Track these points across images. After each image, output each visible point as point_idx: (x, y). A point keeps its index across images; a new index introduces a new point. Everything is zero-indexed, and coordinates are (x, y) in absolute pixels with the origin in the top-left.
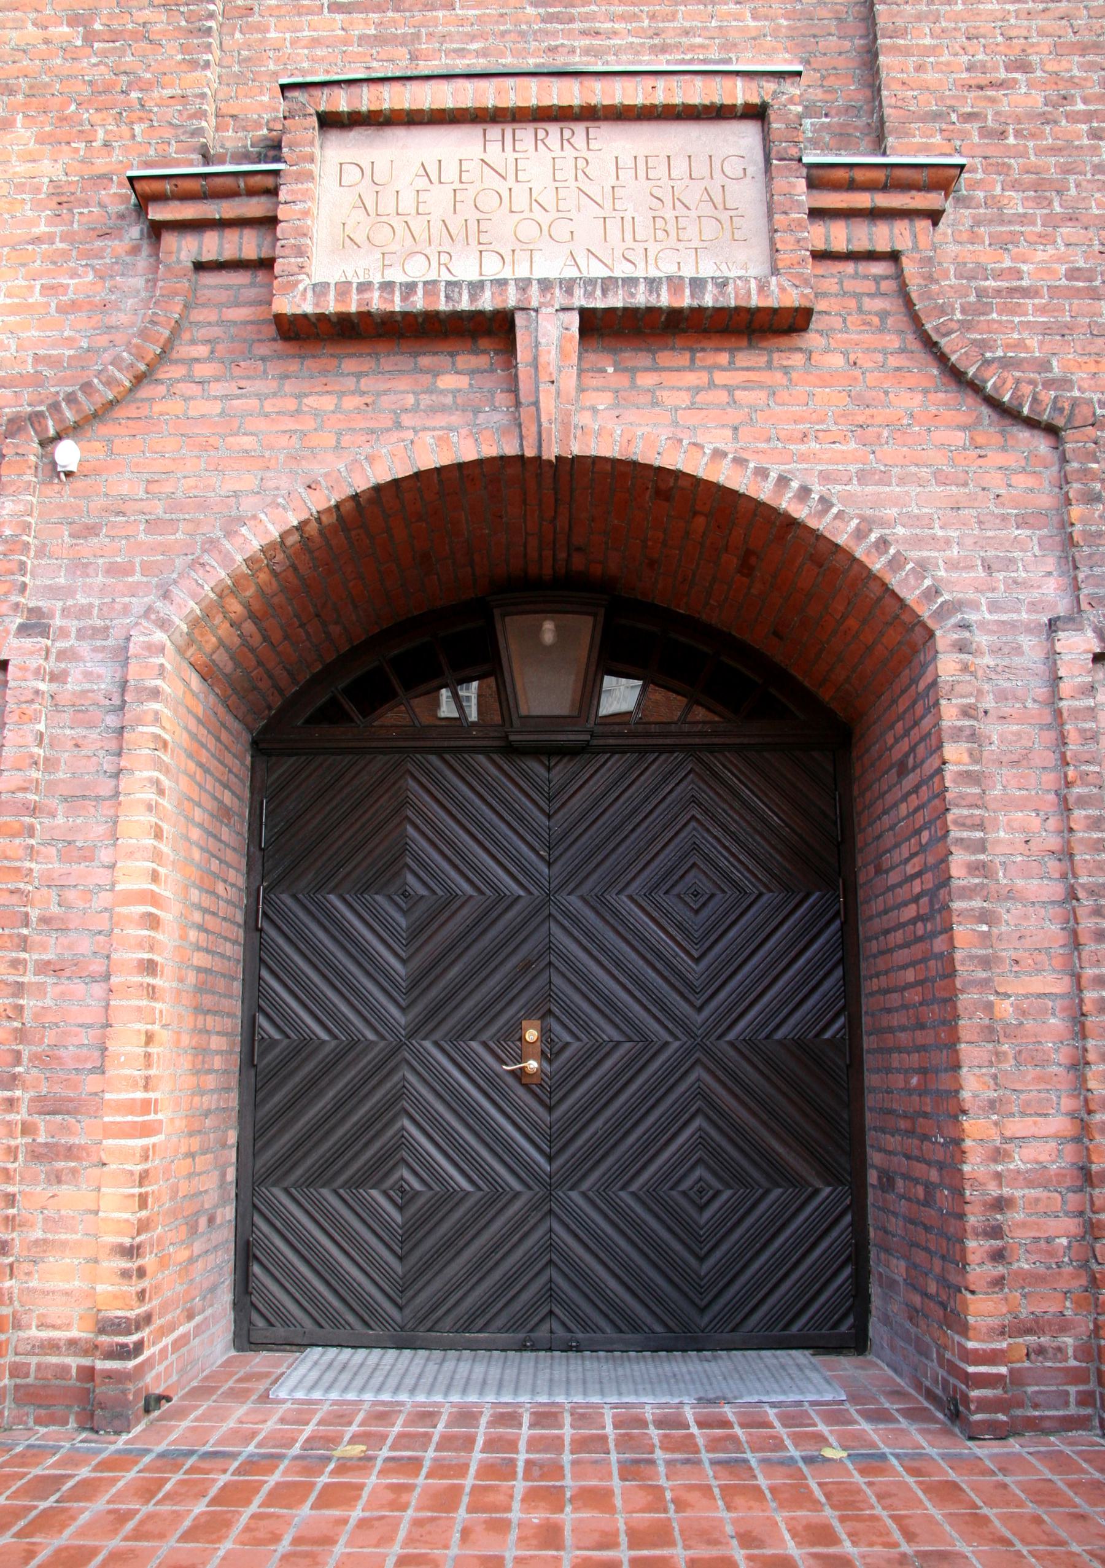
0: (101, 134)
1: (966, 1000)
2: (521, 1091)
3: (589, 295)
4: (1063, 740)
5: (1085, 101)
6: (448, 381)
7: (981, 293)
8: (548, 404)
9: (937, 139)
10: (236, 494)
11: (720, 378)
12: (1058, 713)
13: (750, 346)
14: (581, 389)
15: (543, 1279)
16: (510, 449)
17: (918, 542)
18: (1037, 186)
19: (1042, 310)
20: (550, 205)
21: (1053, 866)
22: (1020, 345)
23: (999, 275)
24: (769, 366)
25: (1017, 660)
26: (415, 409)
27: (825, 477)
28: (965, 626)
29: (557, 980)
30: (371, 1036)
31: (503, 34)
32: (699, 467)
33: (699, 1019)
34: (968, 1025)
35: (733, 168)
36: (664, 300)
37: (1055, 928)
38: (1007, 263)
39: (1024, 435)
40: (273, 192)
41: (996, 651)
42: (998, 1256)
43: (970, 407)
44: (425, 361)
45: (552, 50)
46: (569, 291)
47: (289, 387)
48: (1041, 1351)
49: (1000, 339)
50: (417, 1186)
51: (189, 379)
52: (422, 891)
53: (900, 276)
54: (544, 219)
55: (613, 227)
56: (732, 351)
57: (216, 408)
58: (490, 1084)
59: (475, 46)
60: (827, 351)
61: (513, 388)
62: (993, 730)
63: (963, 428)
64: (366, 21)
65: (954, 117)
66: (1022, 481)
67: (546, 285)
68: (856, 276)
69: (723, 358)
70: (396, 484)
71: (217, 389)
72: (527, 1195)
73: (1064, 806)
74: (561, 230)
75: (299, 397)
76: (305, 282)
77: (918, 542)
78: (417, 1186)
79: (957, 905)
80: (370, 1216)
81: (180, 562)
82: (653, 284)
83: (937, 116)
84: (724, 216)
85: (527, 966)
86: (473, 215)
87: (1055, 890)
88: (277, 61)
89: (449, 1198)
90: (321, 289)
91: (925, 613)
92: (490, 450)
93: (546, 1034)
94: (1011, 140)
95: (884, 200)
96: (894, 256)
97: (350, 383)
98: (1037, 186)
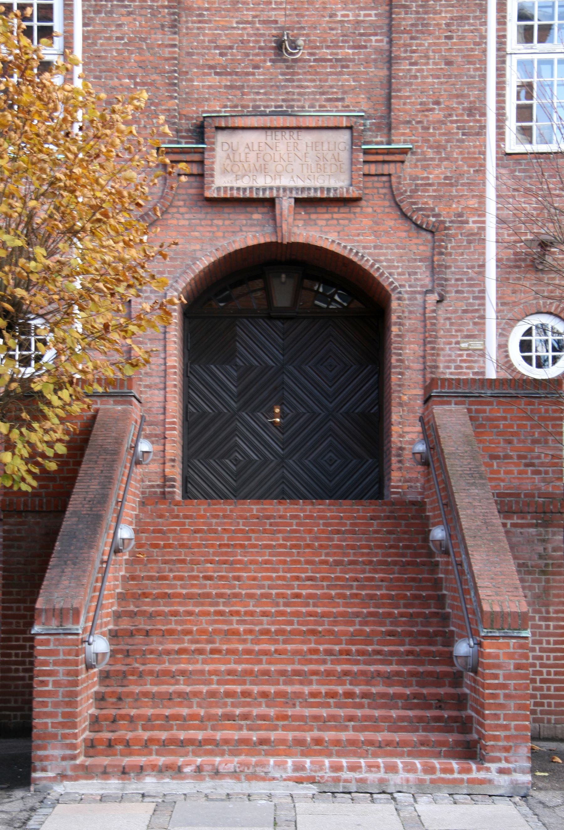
0: (143, 122)
1: (394, 395)
2: (274, 428)
3: (297, 193)
4: (425, 326)
5: (457, 116)
6: (256, 216)
7: (417, 185)
8: (285, 227)
9: (408, 131)
10: (195, 251)
11: (335, 216)
12: (425, 317)
13: (345, 206)
14: (295, 220)
15: (281, 487)
16: (274, 240)
17: (389, 267)
18: (438, 147)
19: (434, 191)
20: (286, 159)
21: (421, 360)
22: (426, 203)
23: (423, 179)
24: (350, 212)
25: (416, 302)
26: (246, 225)
27: (364, 248)
28: (400, 293)
29: (286, 393)
30: (225, 411)
31: (272, 86)
32: (327, 245)
33: (331, 405)
34: (394, 402)
35: (342, 146)
36: (319, 195)
37: (420, 377)
38: (425, 175)
39: (424, 233)
40: (203, 153)
41: (410, 299)
42: (400, 462)
43: (407, 225)
44: (249, 209)
45: (287, 93)
46: (291, 192)
47: (208, 217)
48: (411, 487)
49: (420, 201)
50: (241, 458)
51: (178, 212)
52: (242, 364)
53: (390, 181)
54: (284, 164)
55: (305, 167)
56: (339, 207)
57: (186, 223)
58: (264, 426)
59: (262, 91)
60: (367, 207)
61: (274, 218)
62: (407, 322)
63: (405, 231)
64: (226, 79)
65: (414, 122)
66: (422, 248)
67: (285, 189)
68: (378, 181)
69: (336, 209)
70: (241, 249)
71: (187, 216)
72: (275, 461)
73: (425, 344)
74: (289, 168)
75: (212, 220)
76: (214, 186)
77: (389, 267)
78: (241, 458)
79: (393, 370)
80: (226, 468)
81: (179, 271)
82: (316, 189)
83: (409, 122)
84: (338, 163)
85: (275, 388)
86: (262, 162)
87: (420, 366)
88: (198, 94)
89: (251, 461)
90: (219, 189)
91: (389, 289)
92: (268, 240)
93: (282, 410)
94: (431, 131)
95: (387, 158)
96: (389, 175)
97: (226, 216)
98: (438, 147)
